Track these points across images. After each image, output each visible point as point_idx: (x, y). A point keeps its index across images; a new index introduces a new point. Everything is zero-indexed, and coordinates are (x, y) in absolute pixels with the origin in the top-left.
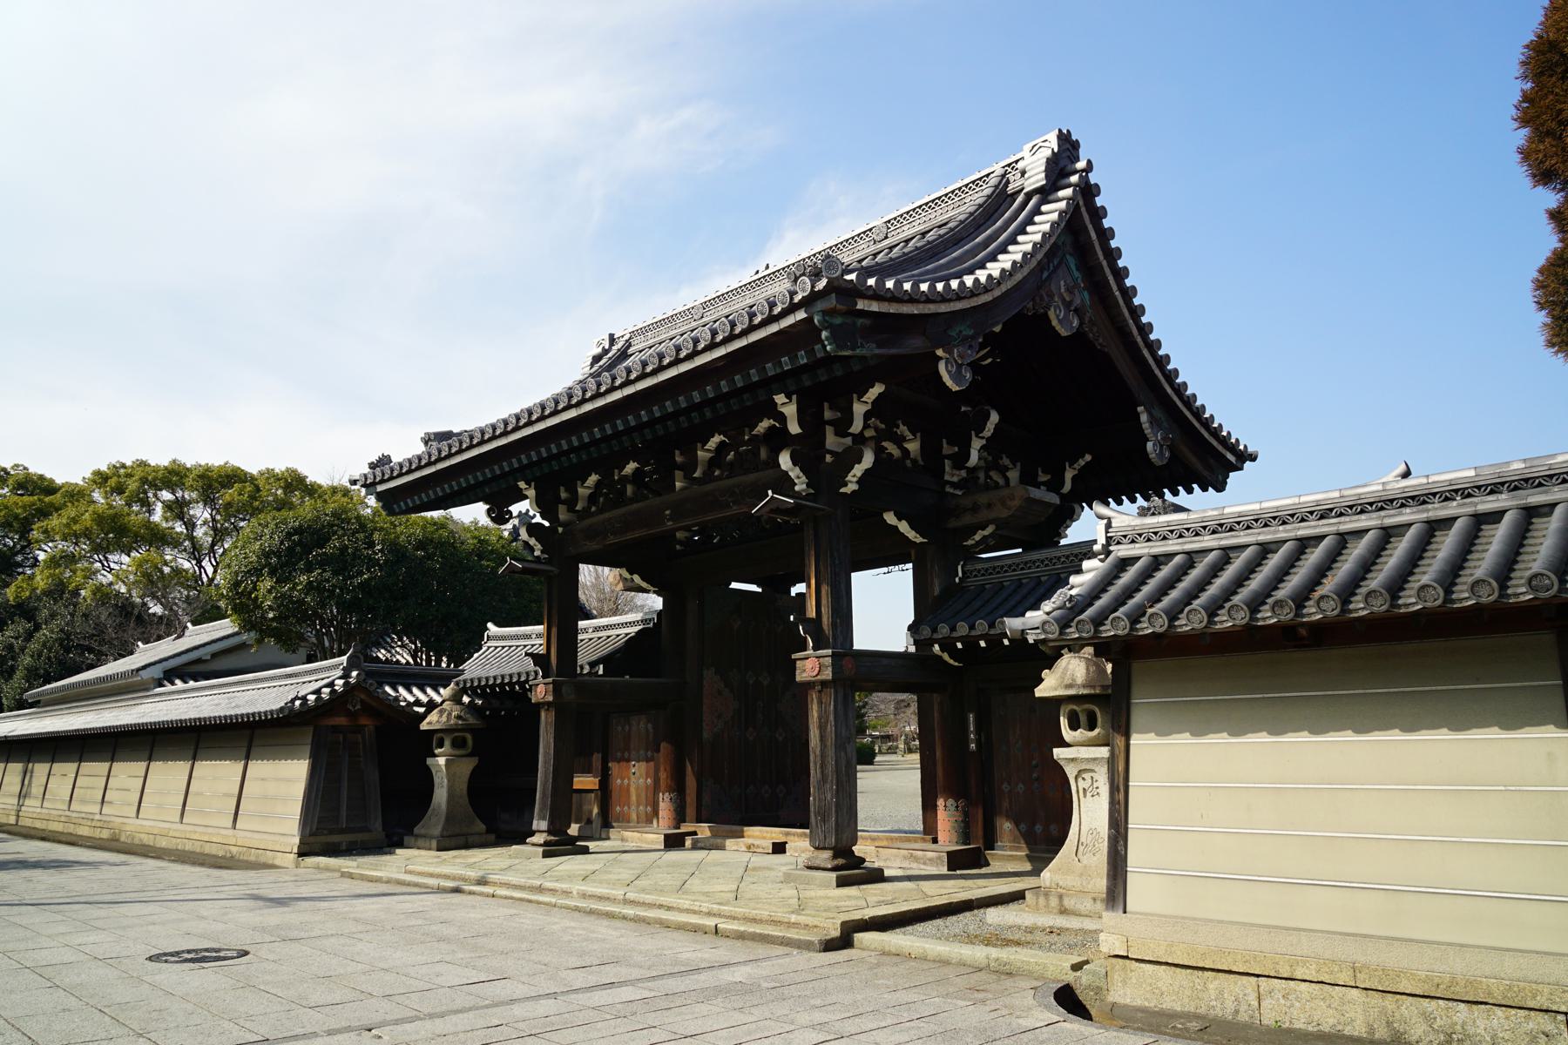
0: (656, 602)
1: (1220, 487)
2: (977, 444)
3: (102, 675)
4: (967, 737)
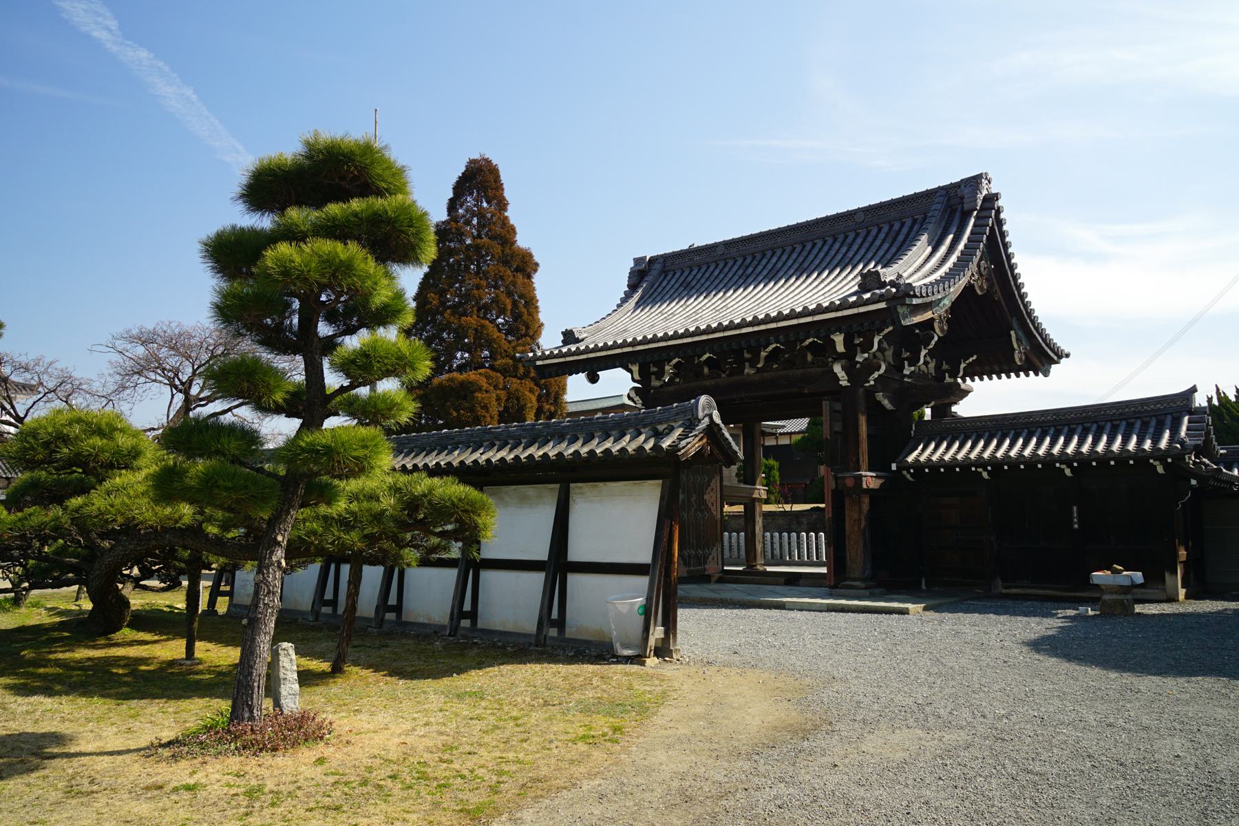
0: (87, 605)
1: (1046, 374)
2: (924, 352)
3: (131, 655)
4: (1072, 517)
